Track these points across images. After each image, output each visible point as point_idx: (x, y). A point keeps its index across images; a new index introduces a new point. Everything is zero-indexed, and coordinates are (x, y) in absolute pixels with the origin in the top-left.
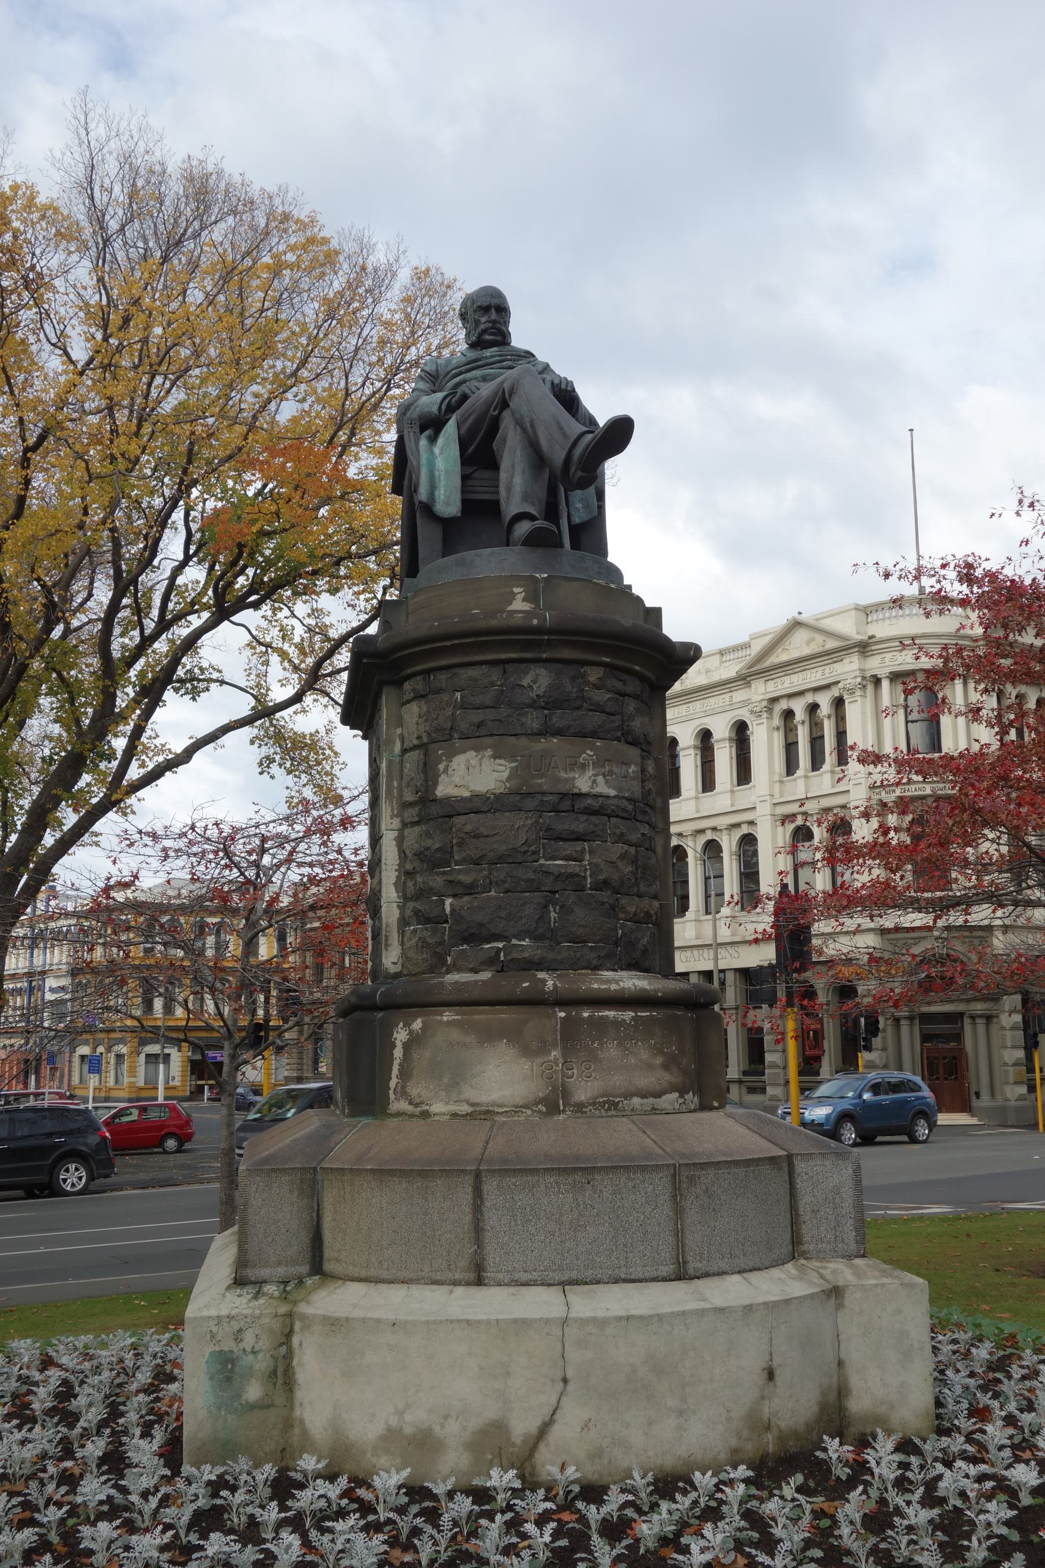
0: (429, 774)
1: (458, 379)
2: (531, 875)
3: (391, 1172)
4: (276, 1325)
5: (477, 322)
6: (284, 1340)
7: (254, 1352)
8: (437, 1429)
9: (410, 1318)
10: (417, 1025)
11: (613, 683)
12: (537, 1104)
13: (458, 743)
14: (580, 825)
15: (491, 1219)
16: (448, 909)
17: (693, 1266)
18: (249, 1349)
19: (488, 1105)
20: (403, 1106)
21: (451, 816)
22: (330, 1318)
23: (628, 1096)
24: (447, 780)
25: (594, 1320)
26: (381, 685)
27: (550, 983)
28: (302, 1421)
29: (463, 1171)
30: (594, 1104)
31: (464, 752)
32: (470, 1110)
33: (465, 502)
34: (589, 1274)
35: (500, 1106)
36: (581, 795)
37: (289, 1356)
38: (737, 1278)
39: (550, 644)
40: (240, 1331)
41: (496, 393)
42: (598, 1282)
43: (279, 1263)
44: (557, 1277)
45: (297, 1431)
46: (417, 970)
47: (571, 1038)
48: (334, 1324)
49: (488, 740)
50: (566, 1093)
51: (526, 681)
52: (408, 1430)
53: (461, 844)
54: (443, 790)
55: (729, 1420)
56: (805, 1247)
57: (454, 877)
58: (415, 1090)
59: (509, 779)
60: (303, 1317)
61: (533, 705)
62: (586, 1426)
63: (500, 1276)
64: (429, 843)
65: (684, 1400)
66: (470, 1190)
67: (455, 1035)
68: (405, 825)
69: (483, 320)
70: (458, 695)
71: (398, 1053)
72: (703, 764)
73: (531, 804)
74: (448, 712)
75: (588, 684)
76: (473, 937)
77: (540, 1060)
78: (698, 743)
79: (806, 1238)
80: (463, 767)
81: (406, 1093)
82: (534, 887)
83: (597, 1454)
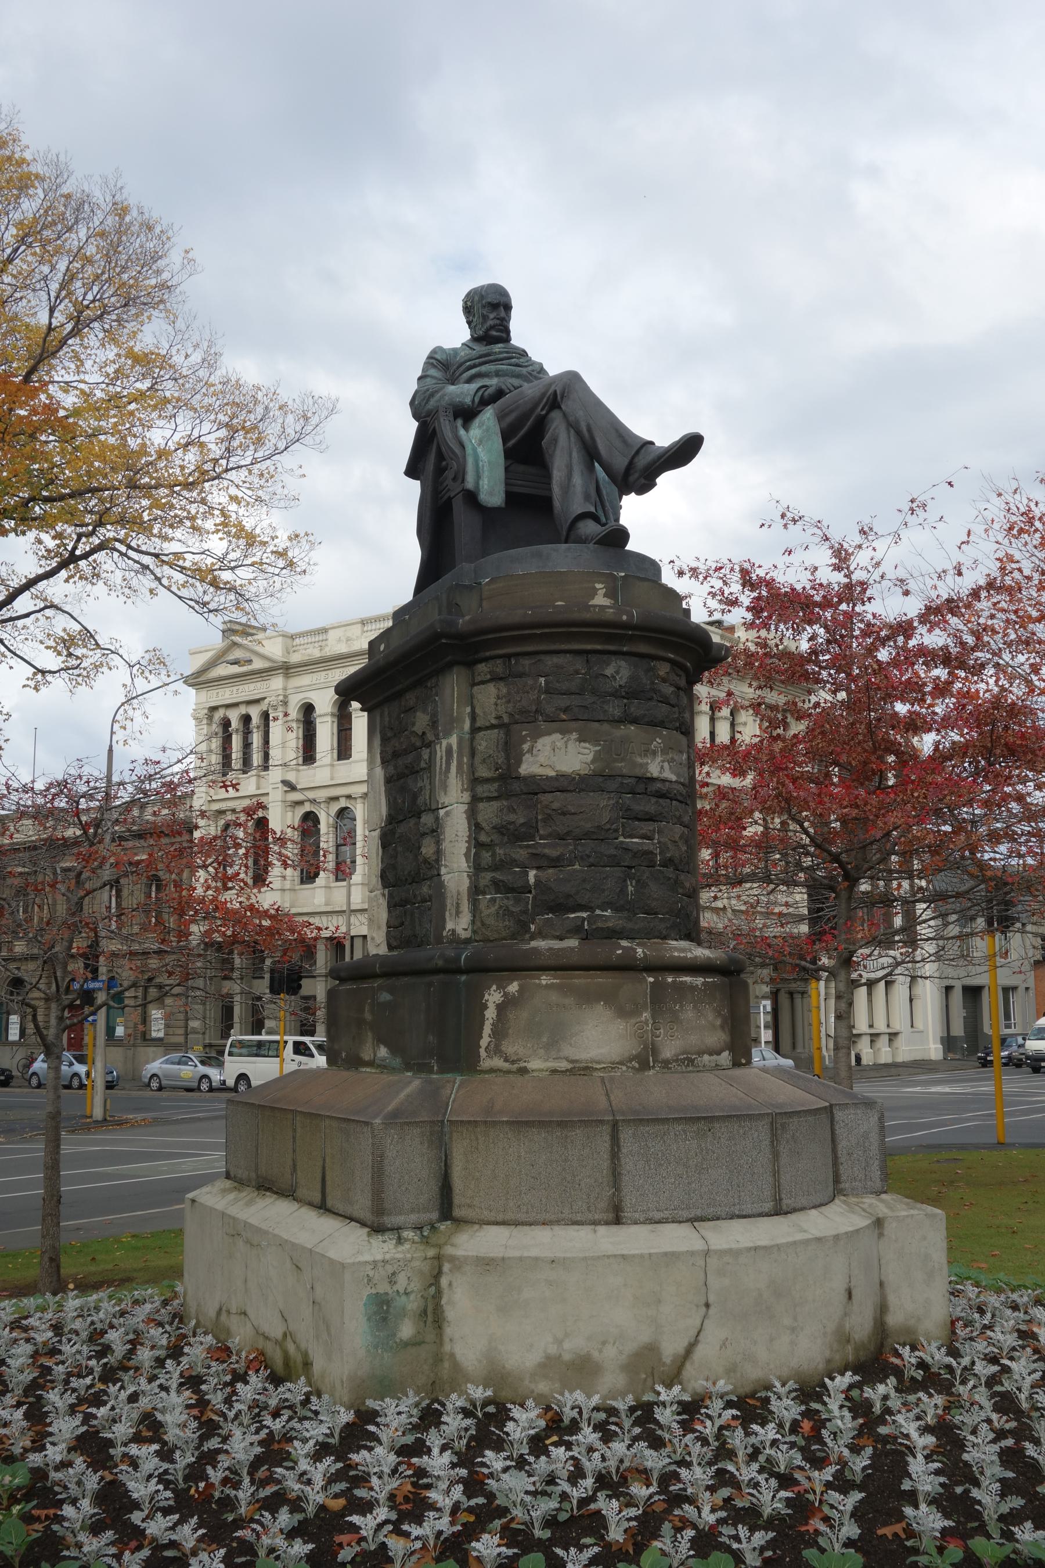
0: (512, 752)
1: (473, 371)
2: (613, 851)
3: (528, 1124)
4: (426, 1267)
5: (485, 318)
6: (432, 1281)
7: (406, 1294)
8: (595, 1354)
9: (568, 1255)
10: (513, 987)
11: (673, 677)
12: (631, 1061)
13: (543, 726)
14: (650, 806)
15: (628, 1163)
16: (532, 880)
17: (787, 1202)
18: (402, 1291)
19: (587, 1061)
20: (498, 1062)
21: (536, 794)
22: (483, 1258)
23: (700, 1053)
24: (531, 759)
25: (729, 1251)
26: (450, 666)
27: (640, 950)
28: (452, 1355)
29: (602, 1122)
30: (677, 1060)
31: (549, 734)
32: (570, 1066)
33: (508, 494)
34: (711, 1211)
35: (598, 1063)
36: (653, 779)
37: (439, 1293)
38: (814, 1212)
39: (631, 639)
40: (394, 1274)
41: (544, 394)
42: (718, 1219)
43: (412, 1211)
44: (685, 1214)
45: (446, 1364)
46: (496, 936)
47: (658, 999)
48: (487, 1264)
49: (574, 725)
50: (655, 1051)
51: (609, 671)
52: (567, 1357)
53: (548, 819)
54: (525, 769)
55: (825, 1334)
56: (842, 1186)
57: (539, 851)
58: (510, 1047)
59: (593, 762)
60: (452, 1259)
61: (615, 694)
62: (724, 1345)
63: (637, 1215)
64: (512, 817)
65: (795, 1319)
66: (607, 1138)
67: (554, 997)
68: (475, 800)
69: (492, 316)
70: (542, 680)
71: (491, 1014)
72: (340, 731)
73: (613, 785)
74: (533, 695)
75: (658, 677)
76: (560, 907)
77: (633, 1021)
78: (335, 711)
79: (844, 1178)
80: (548, 748)
81: (501, 1051)
82: (614, 862)
83: (731, 1371)
